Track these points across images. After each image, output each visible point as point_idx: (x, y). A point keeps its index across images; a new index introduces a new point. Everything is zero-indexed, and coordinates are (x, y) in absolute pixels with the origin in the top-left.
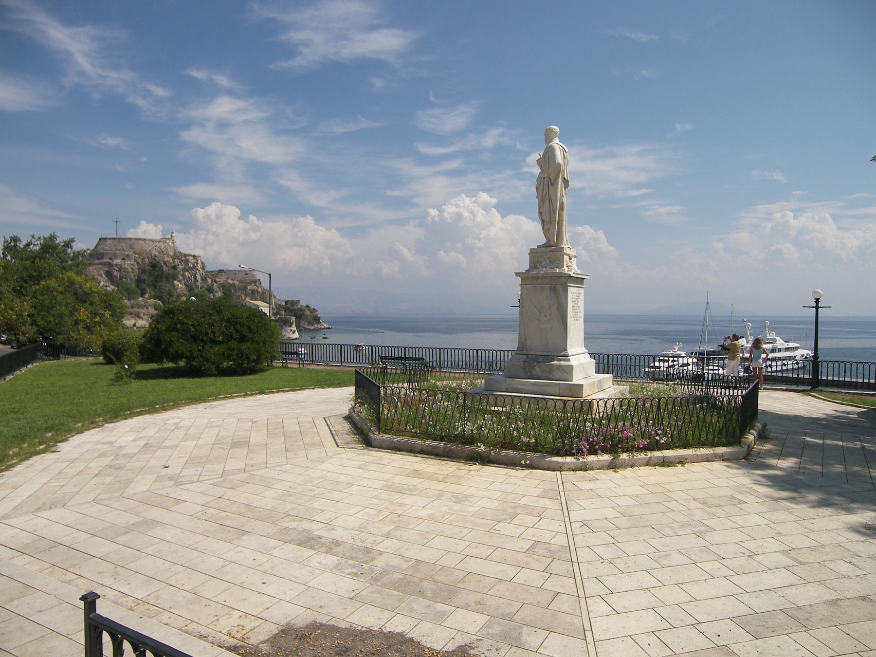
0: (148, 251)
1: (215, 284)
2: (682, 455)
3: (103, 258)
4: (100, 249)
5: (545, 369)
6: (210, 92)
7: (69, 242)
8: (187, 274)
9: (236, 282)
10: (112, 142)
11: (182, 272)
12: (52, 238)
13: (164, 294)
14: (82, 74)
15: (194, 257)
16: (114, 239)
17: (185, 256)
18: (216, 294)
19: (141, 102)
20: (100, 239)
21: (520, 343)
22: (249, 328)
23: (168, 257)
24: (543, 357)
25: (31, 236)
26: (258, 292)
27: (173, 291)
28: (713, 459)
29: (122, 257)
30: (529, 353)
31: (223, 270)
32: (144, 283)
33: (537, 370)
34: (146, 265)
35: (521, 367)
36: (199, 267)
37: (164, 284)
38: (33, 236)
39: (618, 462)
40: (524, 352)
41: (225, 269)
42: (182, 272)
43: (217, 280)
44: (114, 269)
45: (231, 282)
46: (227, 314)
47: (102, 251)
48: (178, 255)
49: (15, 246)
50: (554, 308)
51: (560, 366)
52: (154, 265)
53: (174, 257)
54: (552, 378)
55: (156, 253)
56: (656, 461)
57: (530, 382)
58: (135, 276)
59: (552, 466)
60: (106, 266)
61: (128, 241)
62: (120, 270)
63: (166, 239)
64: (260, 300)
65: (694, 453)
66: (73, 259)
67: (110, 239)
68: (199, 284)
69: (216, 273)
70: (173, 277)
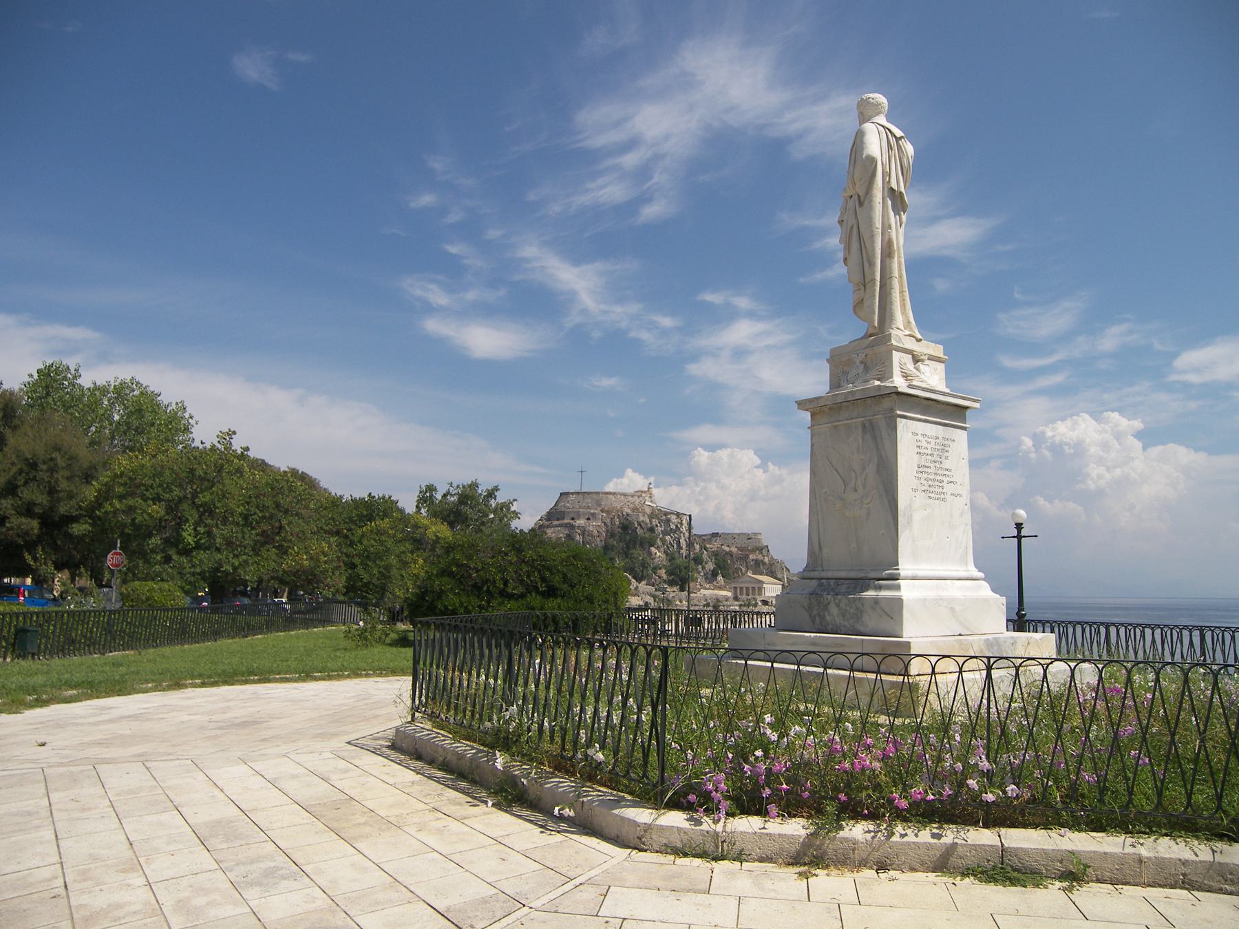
0: (618, 508)
1: (705, 552)
2: (1072, 852)
3: (563, 519)
4: (561, 507)
5: (848, 608)
6: (727, 316)
7: (492, 490)
8: (668, 538)
9: (734, 549)
10: (607, 382)
11: (661, 536)
12: (474, 486)
13: (637, 565)
14: (585, 312)
15: (678, 515)
16: (578, 493)
17: (666, 514)
18: (707, 566)
19: (645, 335)
20: (561, 493)
21: (811, 553)
22: (565, 576)
23: (644, 516)
24: (848, 582)
25: (448, 484)
26: (764, 564)
27: (648, 560)
28: (1215, 885)
29: (587, 517)
30: (824, 575)
31: (718, 533)
32: (613, 550)
33: (833, 614)
34: (617, 526)
35: (803, 607)
36: (684, 528)
37: (638, 554)
38: (451, 484)
39: (830, 847)
40: (816, 574)
41: (720, 532)
42: (661, 536)
43: (708, 546)
44: (576, 532)
45: (727, 549)
46: (529, 554)
47: (563, 509)
48: (656, 513)
49: (431, 496)
50: (871, 469)
51: (876, 601)
52: (626, 526)
53: (651, 517)
54: (862, 629)
55: (629, 511)
56: (971, 861)
57: (807, 637)
58: (601, 541)
59: (626, 832)
60: (567, 529)
61: (595, 496)
62: (583, 533)
63: (642, 492)
64: (766, 575)
65: (1129, 850)
66: (495, 511)
67: (573, 493)
68: (683, 552)
69: (709, 537)
70: (649, 542)
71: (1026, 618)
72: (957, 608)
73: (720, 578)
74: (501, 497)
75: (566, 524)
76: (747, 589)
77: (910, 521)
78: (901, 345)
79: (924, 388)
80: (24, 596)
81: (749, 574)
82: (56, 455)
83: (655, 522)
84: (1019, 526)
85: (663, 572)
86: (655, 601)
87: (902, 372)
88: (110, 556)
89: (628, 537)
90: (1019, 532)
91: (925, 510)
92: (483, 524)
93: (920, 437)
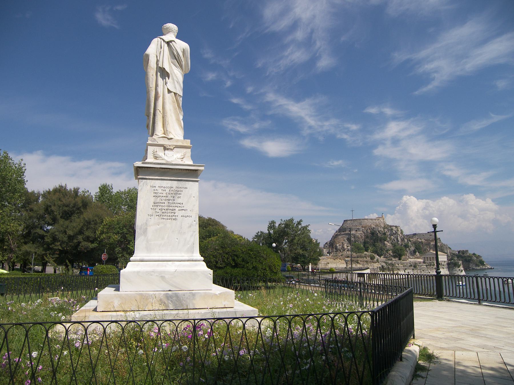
1: (410, 242)
8: (392, 237)
9: (423, 240)
12: (291, 220)
13: (378, 249)
15: (396, 227)
16: (351, 220)
17: (391, 226)
18: (411, 248)
32: (368, 244)
36: (399, 233)
37: (379, 244)
41: (417, 233)
43: (411, 239)
45: (420, 240)
48: (386, 227)
49: (274, 225)
52: (373, 233)
53: (384, 228)
55: (374, 226)
61: (358, 221)
62: (354, 237)
67: (349, 220)
68: (400, 242)
71: (441, 274)
72: (167, 276)
73: (417, 253)
74: (303, 224)
75: (347, 233)
76: (430, 258)
77: (145, 231)
78: (156, 143)
79: (155, 163)
80: (89, 271)
81: (431, 251)
82: (97, 218)
83: (386, 230)
84: (435, 226)
85: (390, 252)
86: (386, 265)
87: (154, 156)
88: (103, 255)
89: (374, 238)
90: (435, 229)
91: (158, 225)
92: (296, 236)
93: (157, 188)
